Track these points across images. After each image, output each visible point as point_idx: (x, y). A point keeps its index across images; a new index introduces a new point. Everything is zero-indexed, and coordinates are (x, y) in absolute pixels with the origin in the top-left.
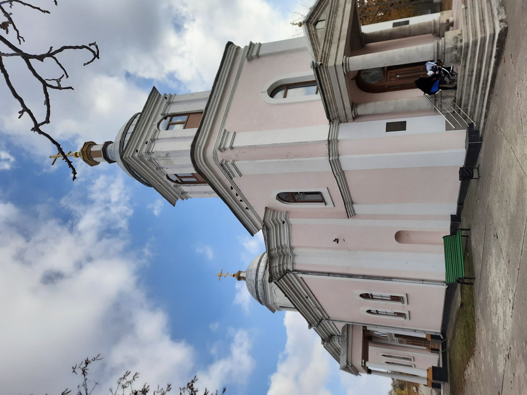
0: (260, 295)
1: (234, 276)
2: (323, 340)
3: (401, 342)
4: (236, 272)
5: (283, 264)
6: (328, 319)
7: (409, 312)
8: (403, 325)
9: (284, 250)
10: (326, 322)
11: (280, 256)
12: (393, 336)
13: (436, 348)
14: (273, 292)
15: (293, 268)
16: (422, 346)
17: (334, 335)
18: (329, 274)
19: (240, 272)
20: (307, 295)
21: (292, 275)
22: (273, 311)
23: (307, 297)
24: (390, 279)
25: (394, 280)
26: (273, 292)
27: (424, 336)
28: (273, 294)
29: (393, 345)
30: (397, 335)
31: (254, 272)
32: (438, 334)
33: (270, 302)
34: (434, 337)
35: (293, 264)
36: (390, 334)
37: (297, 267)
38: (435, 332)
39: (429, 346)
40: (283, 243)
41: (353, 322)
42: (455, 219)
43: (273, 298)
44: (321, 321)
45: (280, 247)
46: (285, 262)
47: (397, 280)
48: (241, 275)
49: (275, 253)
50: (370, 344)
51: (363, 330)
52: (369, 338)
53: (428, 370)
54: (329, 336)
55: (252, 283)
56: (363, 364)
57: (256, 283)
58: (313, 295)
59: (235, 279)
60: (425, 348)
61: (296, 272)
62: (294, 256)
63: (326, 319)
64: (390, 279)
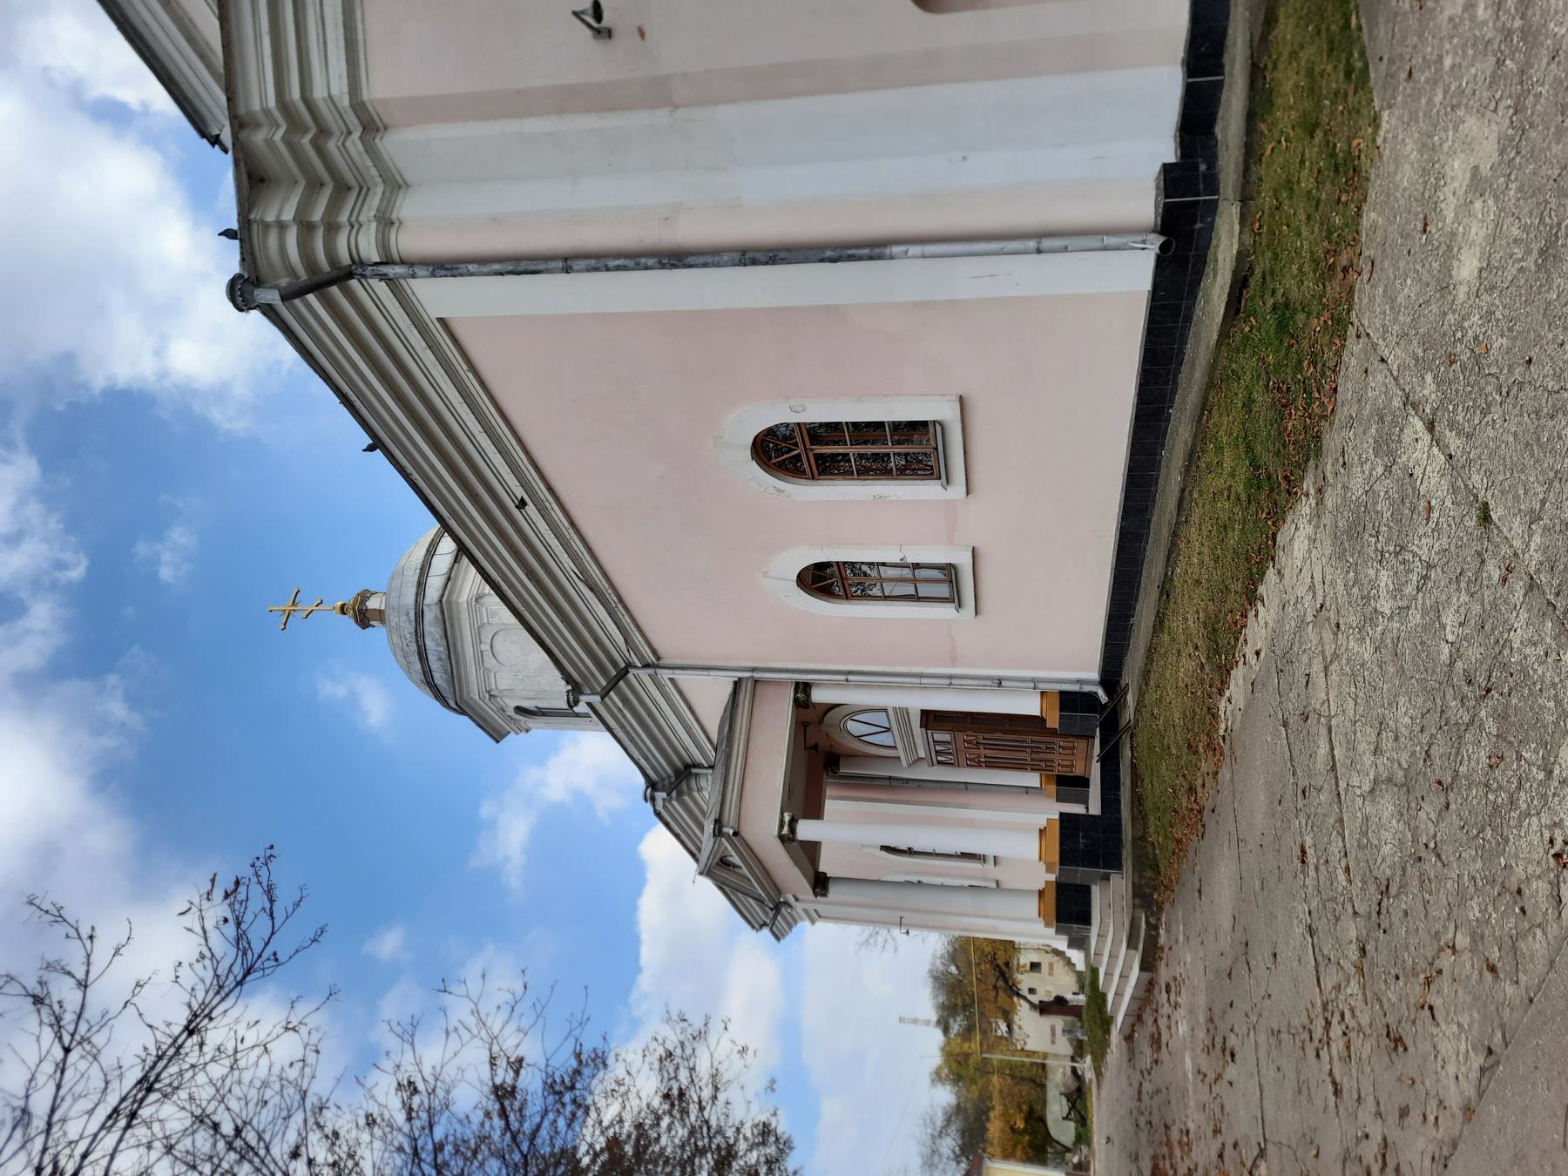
0: (434, 664)
1: (343, 610)
2: (652, 785)
3: (941, 757)
4: (348, 597)
5: (332, 228)
6: (654, 664)
7: (962, 400)
8: (954, 663)
9: (332, 146)
10: (644, 675)
11: (315, 185)
12: (916, 720)
13: (1078, 771)
14: (485, 647)
15: (383, 245)
16: (1019, 766)
17: (699, 766)
18: (567, 262)
19: (365, 596)
20: (520, 493)
21: (381, 288)
22: (497, 735)
23: (522, 504)
24: (873, 250)
25: (896, 249)
26: (485, 647)
27: (1028, 705)
28: (488, 656)
29: (921, 785)
30: (931, 719)
31: (413, 578)
32: (1086, 689)
33: (474, 692)
34: (1072, 701)
35: (386, 222)
36: (903, 713)
37: (409, 242)
38: (1079, 681)
39: (1049, 768)
40: (319, 93)
41: (754, 670)
42: (1174, 179)
43: (487, 671)
44: (623, 674)
45: (305, 119)
46: (343, 218)
47: (914, 250)
48: (373, 604)
49: (269, 142)
50: (829, 792)
51: (796, 700)
52: (825, 757)
53: (1041, 893)
54: (677, 773)
55: (404, 618)
56: (786, 830)
57: (419, 615)
58: (550, 489)
59: (348, 621)
60: (1032, 779)
61: (399, 270)
62: (395, 185)
63: (647, 666)
64: (873, 250)
